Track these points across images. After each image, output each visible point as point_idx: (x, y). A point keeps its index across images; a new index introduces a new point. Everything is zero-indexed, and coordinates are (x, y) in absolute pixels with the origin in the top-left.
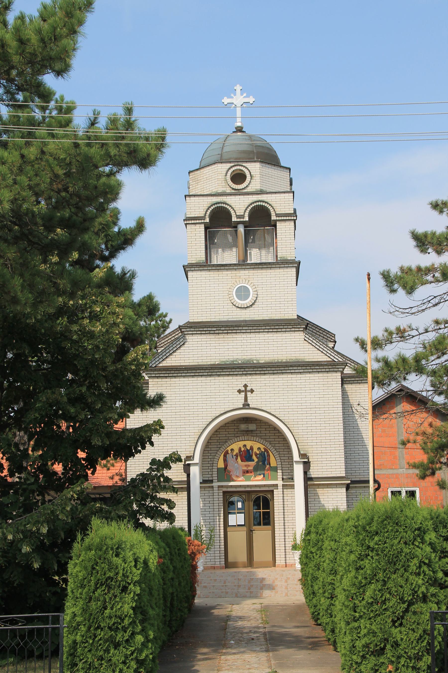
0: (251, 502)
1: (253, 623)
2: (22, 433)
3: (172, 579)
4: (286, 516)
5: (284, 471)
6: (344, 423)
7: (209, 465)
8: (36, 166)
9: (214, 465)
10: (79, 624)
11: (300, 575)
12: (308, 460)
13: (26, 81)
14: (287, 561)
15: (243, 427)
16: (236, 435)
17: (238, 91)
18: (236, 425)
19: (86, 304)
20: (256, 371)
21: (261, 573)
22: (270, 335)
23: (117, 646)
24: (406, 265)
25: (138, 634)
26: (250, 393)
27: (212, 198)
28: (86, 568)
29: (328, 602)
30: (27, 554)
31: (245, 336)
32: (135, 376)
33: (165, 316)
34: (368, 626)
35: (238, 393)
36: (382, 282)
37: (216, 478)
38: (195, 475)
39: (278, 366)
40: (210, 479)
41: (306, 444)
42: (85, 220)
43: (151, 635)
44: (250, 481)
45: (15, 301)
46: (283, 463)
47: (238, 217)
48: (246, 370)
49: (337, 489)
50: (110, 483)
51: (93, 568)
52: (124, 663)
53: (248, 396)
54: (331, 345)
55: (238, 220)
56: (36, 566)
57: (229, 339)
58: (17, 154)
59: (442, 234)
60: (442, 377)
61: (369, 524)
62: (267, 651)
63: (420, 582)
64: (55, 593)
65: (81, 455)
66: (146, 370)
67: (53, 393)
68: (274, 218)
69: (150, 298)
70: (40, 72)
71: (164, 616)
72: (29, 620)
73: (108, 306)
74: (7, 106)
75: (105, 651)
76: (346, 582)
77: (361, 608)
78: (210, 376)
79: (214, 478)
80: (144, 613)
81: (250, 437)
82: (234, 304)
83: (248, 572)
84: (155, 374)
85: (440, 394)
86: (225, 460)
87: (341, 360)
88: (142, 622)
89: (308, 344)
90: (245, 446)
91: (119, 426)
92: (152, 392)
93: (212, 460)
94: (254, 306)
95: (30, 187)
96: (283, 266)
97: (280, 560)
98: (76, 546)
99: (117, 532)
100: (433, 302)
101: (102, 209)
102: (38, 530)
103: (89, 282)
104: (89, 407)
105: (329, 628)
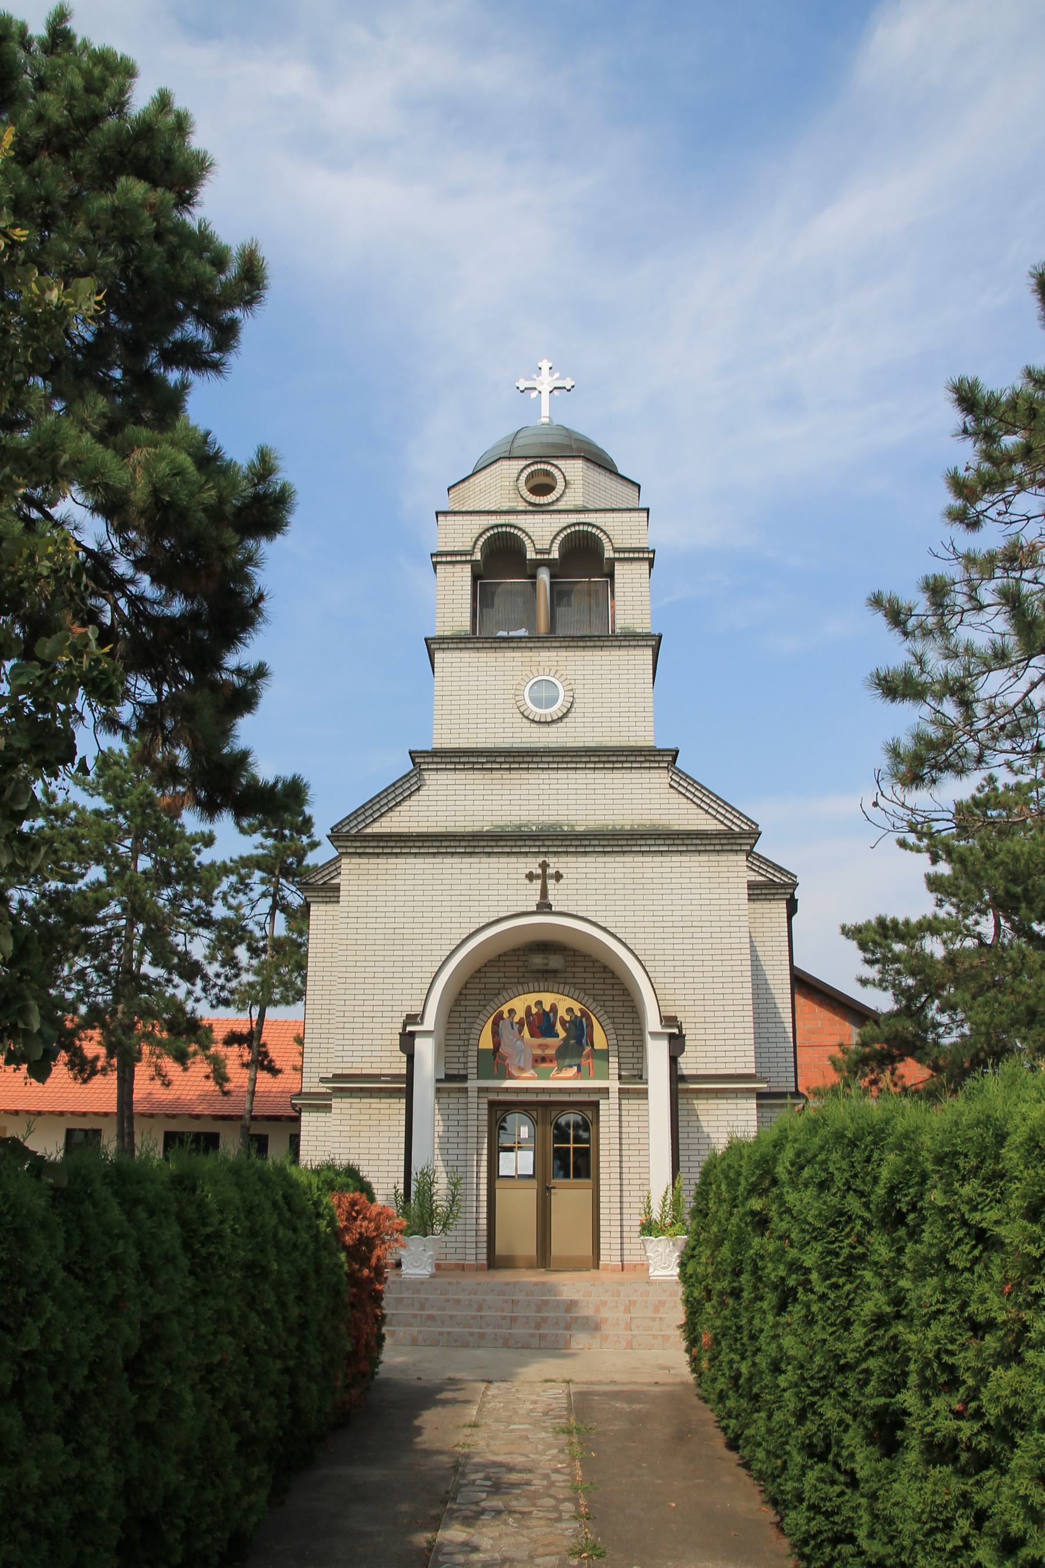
0: (548, 1127)
4: (624, 1159)
5: (622, 1060)
7: (461, 1043)
9: (471, 1042)
12: (680, 1031)
14: (625, 1258)
16: (521, 980)
18: (521, 958)
20: (567, 846)
22: (599, 775)
26: (553, 881)
27: (489, 517)
31: (547, 776)
35: (527, 881)
37: (475, 1071)
40: (462, 1072)
41: (672, 1003)
44: (549, 1078)
46: (620, 1043)
47: (538, 552)
48: (547, 843)
49: (738, 1101)
53: (549, 887)
55: (539, 557)
57: (513, 782)
68: (609, 554)
78: (471, 854)
79: (470, 1071)
81: (551, 984)
82: (526, 714)
83: (536, 1284)
84: (356, 847)
86: (495, 1033)
87: (747, 828)
89: (677, 796)
90: (539, 1003)
93: (467, 1031)
94: (565, 720)
96: (627, 643)
97: (609, 1254)
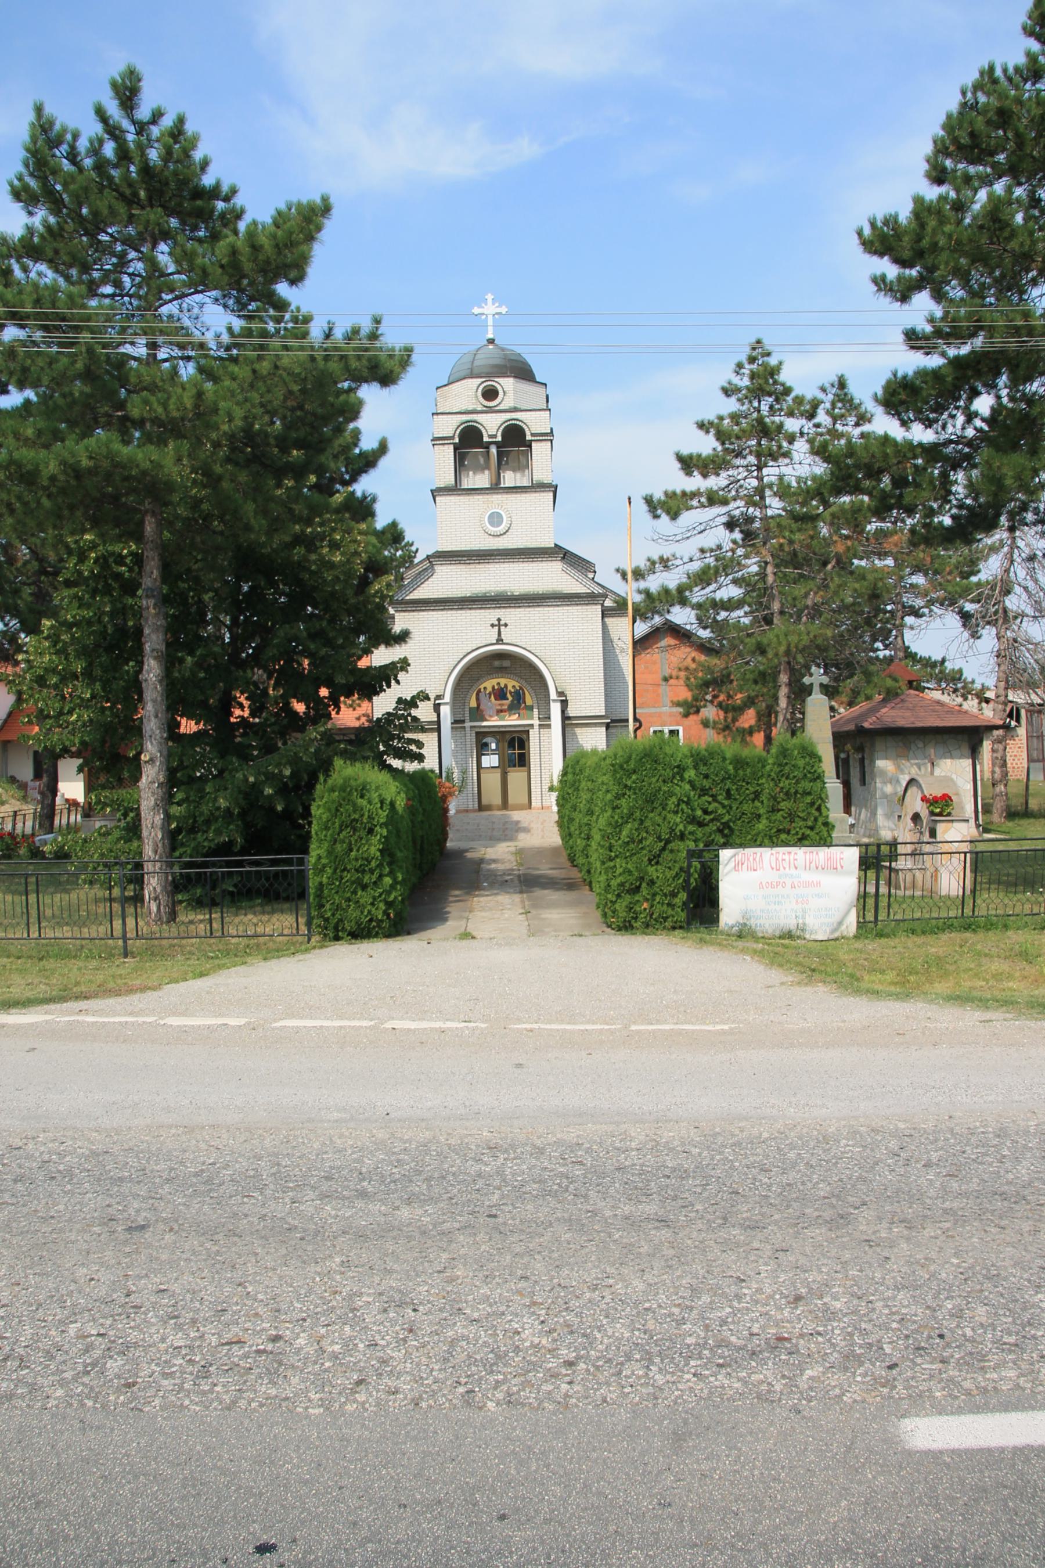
1: (507, 866)
2: (260, 672)
3: (422, 822)
6: (604, 659)
8: (269, 382)
10: (324, 866)
11: (556, 817)
13: (258, 291)
15: (497, 663)
17: (490, 301)
19: (324, 532)
21: (516, 815)
22: (525, 565)
23: (364, 887)
24: (670, 489)
25: (386, 875)
28: (329, 810)
29: (584, 842)
30: (270, 796)
32: (379, 609)
33: (412, 545)
34: (624, 865)
36: (645, 508)
38: (446, 715)
39: (534, 599)
42: (321, 442)
43: (400, 877)
45: (248, 528)
47: (490, 436)
50: (357, 724)
51: (337, 810)
52: (372, 904)
54: (591, 575)
56: (279, 808)
58: (248, 369)
59: (708, 457)
60: (708, 611)
61: (627, 762)
62: (521, 892)
63: (678, 820)
64: (300, 836)
65: (324, 692)
66: (391, 603)
67: (292, 628)
68: (528, 437)
69: (394, 525)
70: (275, 280)
71: (414, 859)
72: (274, 863)
73: (349, 534)
74: (239, 316)
75: (352, 893)
76: (602, 822)
77: (618, 848)
78: (461, 609)
80: (392, 855)
85: (705, 628)
86: (478, 699)
88: (390, 864)
91: (363, 663)
92: (397, 628)
95: (262, 405)
97: (536, 802)
98: (318, 787)
99: (361, 773)
100: (699, 529)
101: (339, 430)
102: (281, 771)
103: (327, 508)
104: (329, 643)
105: (585, 868)
